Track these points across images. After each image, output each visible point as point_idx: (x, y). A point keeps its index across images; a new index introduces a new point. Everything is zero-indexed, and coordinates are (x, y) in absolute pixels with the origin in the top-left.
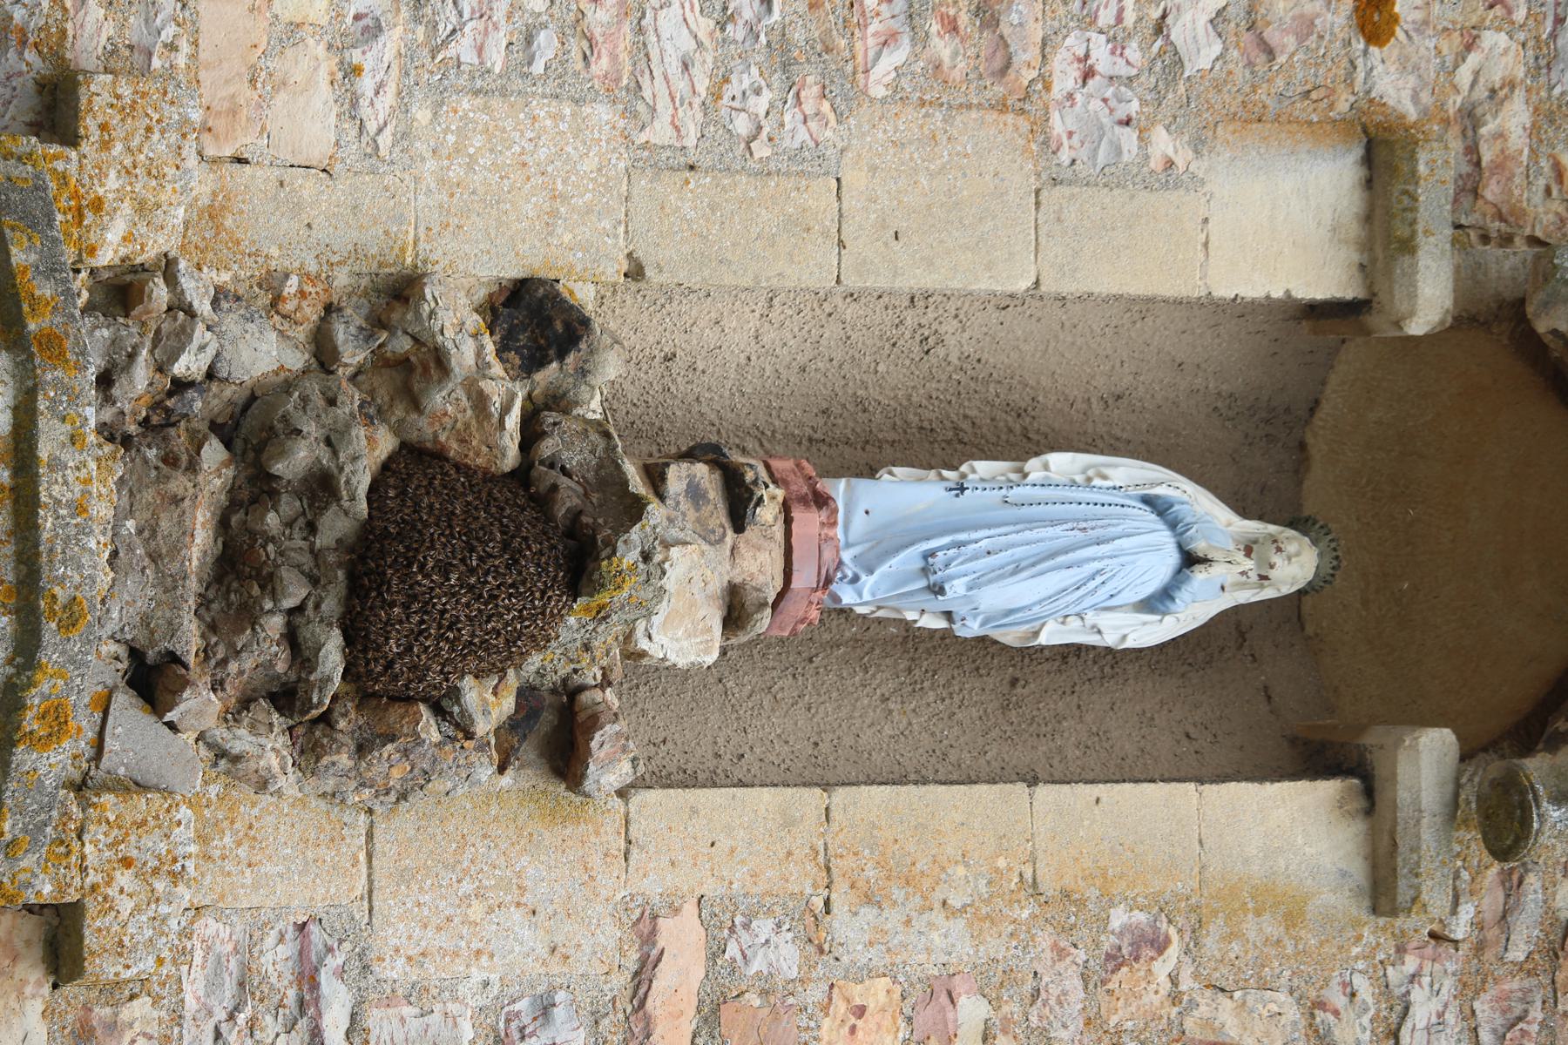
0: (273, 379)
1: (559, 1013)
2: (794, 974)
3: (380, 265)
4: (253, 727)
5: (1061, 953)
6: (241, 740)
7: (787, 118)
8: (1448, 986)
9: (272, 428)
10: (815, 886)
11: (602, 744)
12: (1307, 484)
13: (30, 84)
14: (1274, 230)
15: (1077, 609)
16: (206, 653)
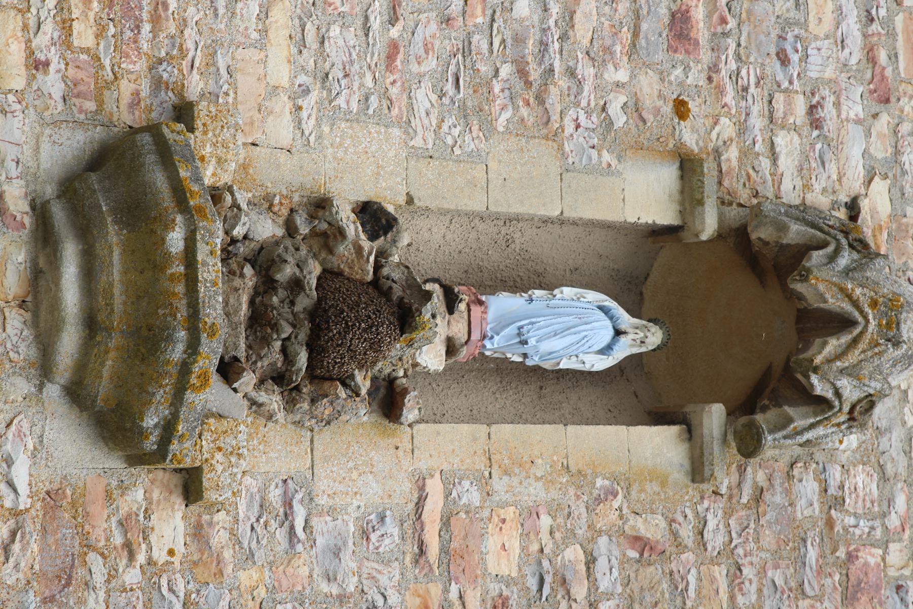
0: (271, 239)
1: (388, 520)
2: (478, 504)
4: (266, 391)
6: (262, 397)
7: (466, 138)
8: (720, 513)
9: (273, 260)
10: (485, 466)
11: (410, 401)
12: (643, 309)
13: (170, 106)
14: (645, 196)
15: (575, 353)
16: (248, 358)
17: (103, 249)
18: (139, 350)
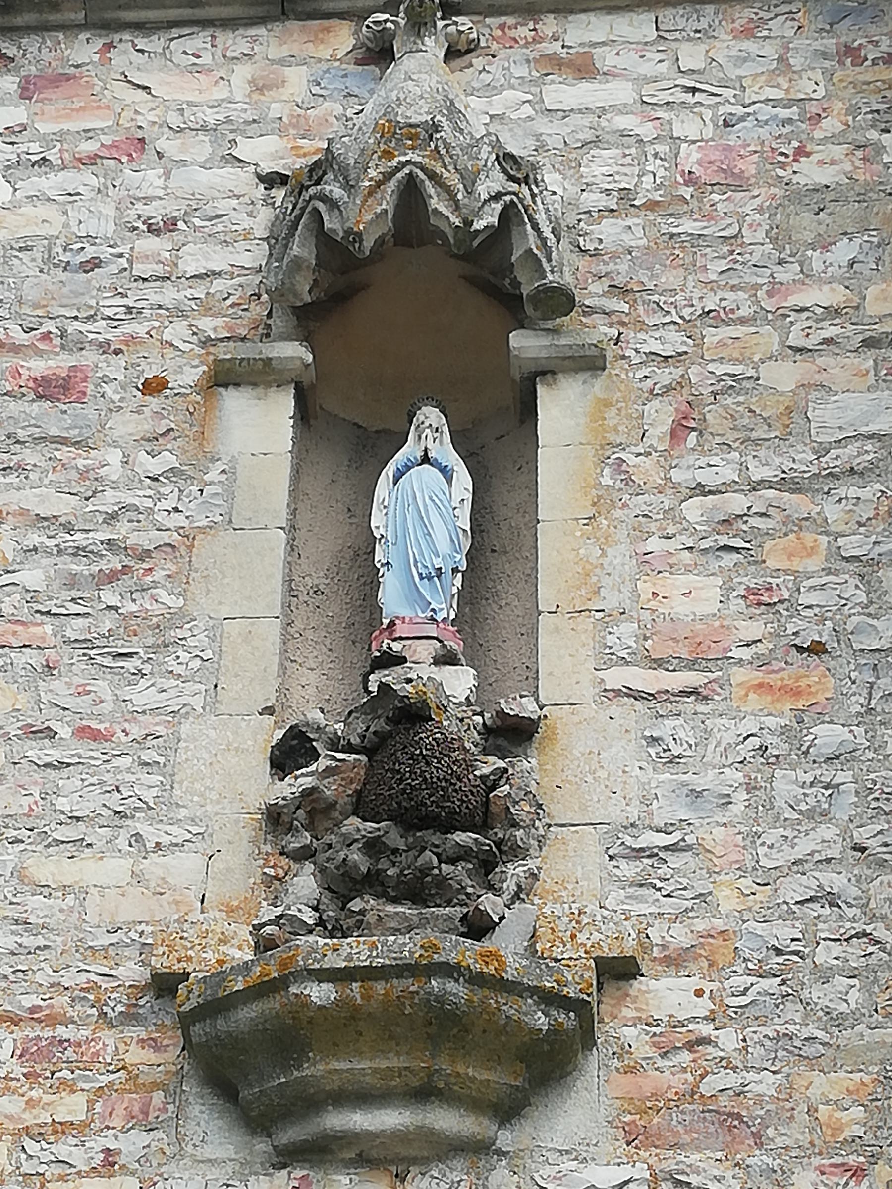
3: (261, 830)
5: (625, 505)
6: (510, 886)
8: (641, 336)
10: (590, 617)
11: (512, 709)
14: (261, 428)
17: (333, 1080)
18: (454, 1036)
